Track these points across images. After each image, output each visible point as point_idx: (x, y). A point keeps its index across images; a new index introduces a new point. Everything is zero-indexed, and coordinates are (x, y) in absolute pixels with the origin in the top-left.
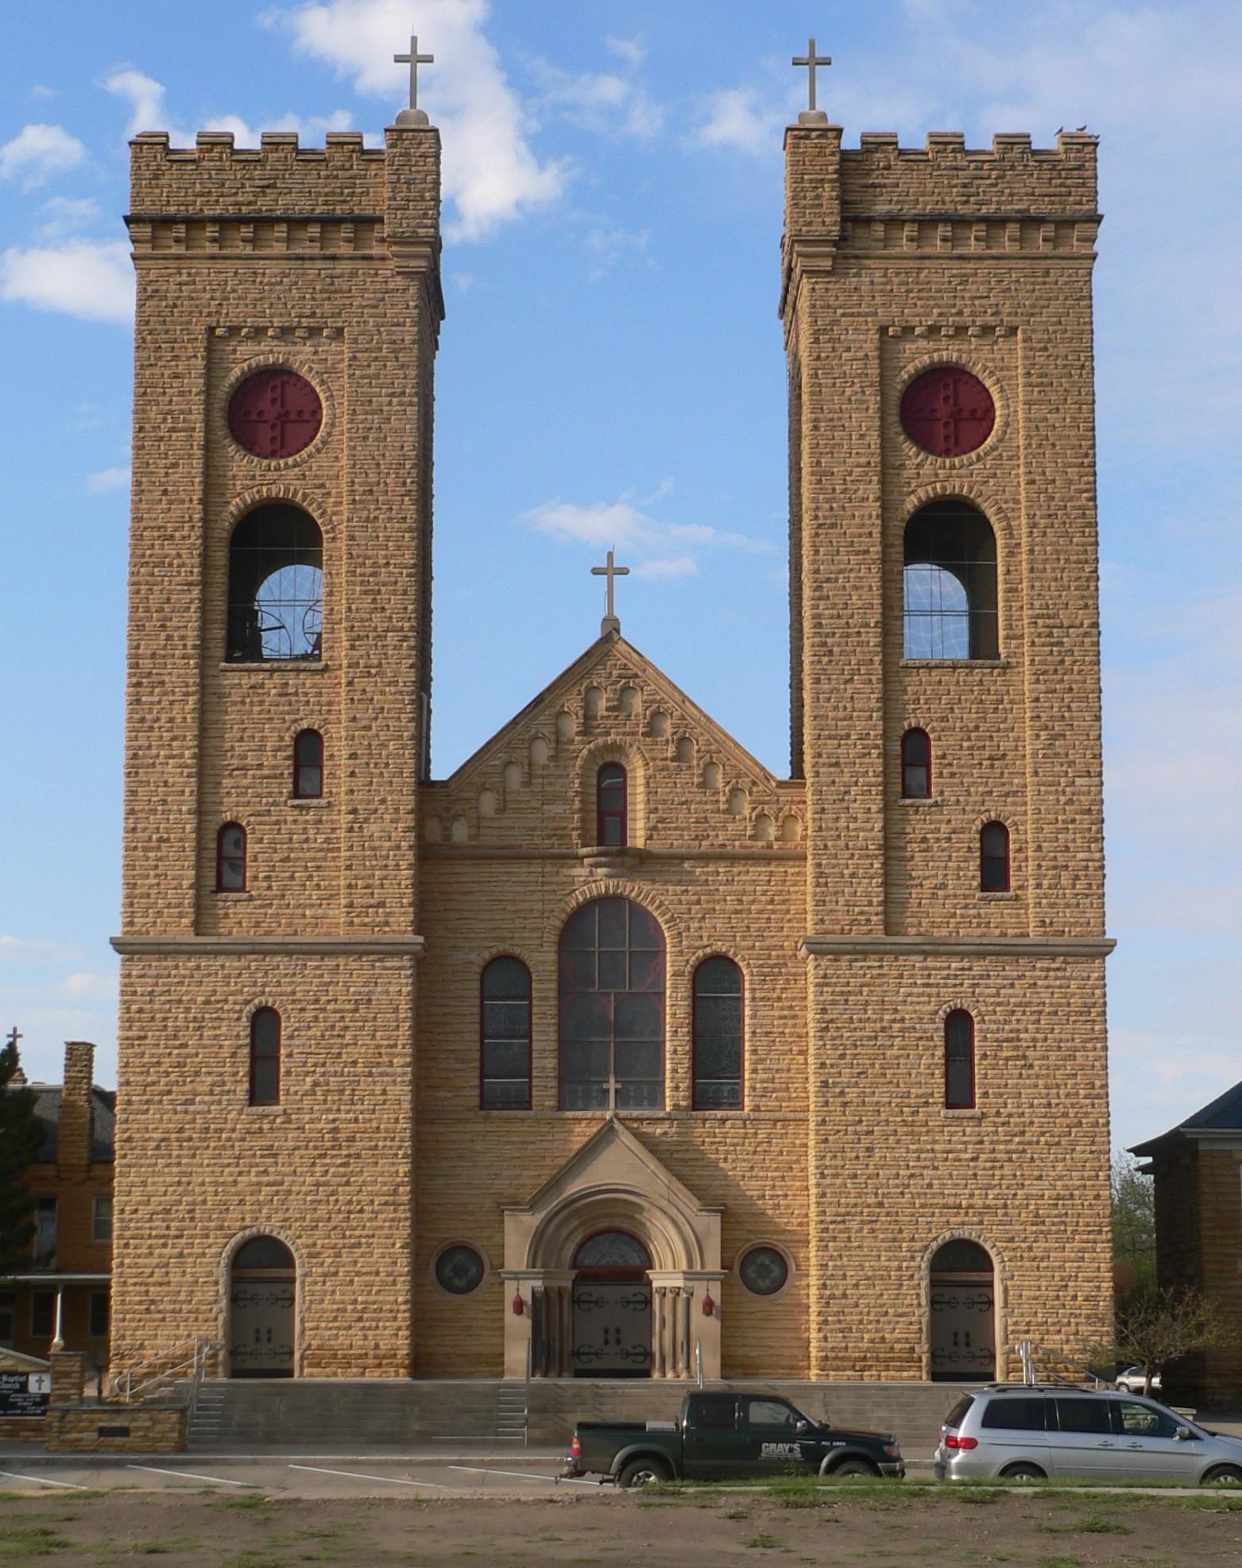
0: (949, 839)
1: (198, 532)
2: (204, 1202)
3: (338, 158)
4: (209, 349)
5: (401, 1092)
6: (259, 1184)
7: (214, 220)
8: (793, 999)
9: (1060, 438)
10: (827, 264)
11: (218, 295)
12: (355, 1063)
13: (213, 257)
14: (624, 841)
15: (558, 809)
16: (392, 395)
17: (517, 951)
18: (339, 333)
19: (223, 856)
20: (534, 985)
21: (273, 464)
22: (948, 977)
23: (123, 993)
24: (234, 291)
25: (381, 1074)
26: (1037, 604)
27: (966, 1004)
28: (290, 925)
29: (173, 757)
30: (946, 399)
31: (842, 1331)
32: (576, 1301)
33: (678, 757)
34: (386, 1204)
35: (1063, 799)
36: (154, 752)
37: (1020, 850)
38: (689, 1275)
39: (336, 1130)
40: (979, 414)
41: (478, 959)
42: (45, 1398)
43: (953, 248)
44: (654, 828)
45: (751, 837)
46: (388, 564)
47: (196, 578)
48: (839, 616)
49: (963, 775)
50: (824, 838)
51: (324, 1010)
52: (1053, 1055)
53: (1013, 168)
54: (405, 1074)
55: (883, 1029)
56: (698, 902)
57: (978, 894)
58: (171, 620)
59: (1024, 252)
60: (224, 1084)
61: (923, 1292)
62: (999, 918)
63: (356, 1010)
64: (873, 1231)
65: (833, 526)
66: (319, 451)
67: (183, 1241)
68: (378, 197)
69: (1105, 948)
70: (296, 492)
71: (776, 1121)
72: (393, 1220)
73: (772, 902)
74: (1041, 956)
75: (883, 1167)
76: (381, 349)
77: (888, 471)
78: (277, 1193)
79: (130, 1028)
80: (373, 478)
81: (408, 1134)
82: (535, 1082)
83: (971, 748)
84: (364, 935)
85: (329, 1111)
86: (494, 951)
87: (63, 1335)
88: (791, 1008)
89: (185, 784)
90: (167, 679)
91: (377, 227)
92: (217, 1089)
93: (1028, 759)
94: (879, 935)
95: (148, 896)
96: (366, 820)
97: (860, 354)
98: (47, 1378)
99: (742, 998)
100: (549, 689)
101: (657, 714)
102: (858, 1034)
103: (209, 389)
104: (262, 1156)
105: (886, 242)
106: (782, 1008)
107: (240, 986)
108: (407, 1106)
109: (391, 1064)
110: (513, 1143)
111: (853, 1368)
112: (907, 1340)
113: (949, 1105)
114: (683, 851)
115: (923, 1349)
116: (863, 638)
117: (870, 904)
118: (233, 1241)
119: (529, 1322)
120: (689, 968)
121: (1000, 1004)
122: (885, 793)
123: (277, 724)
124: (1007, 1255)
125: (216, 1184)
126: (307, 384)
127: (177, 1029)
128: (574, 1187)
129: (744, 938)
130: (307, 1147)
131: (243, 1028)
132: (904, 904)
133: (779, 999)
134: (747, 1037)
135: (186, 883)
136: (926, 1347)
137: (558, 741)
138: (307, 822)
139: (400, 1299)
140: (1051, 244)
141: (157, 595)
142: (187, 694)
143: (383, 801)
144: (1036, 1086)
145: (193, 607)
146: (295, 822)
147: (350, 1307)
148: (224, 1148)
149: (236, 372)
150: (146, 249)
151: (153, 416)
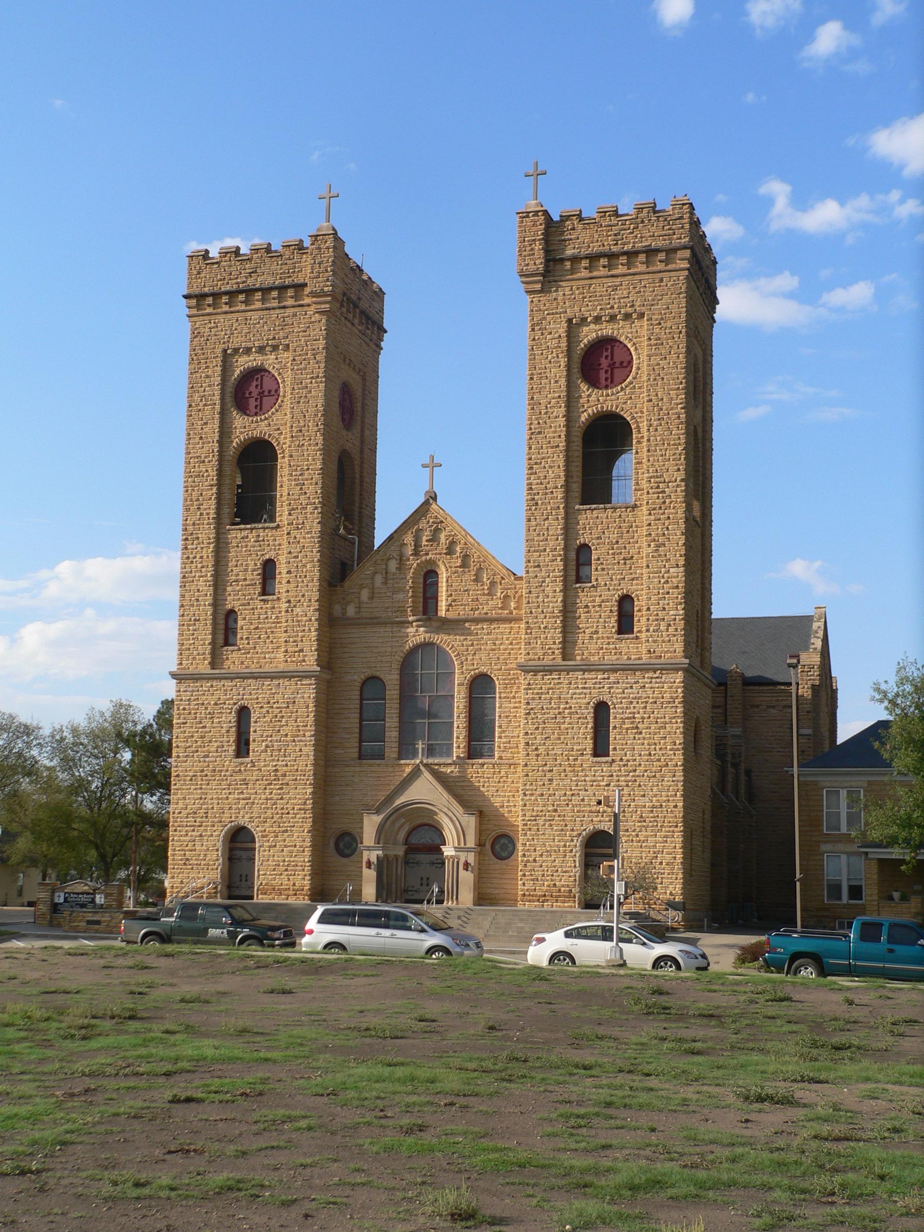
0: (600, 606)
2: (213, 808)
6: (238, 799)
7: (226, 293)
11: (228, 332)
12: (286, 735)
13: (226, 313)
15: (400, 596)
16: (312, 378)
17: (378, 674)
18: (288, 345)
19: (225, 628)
22: (595, 683)
25: (299, 741)
27: (606, 698)
28: (258, 663)
31: (533, 880)
32: (407, 863)
34: (300, 809)
35: (662, 581)
36: (193, 574)
39: (276, 770)
41: (358, 678)
44: (450, 605)
46: (308, 469)
47: (215, 482)
48: (541, 484)
49: (609, 569)
52: (653, 726)
53: (643, 222)
54: (311, 741)
57: (616, 636)
60: (223, 746)
65: (540, 433)
66: (277, 411)
71: (510, 765)
73: (511, 644)
74: (648, 670)
75: (557, 790)
78: (247, 804)
83: (613, 554)
84: (292, 667)
85: (273, 760)
90: (200, 536)
92: (220, 750)
94: (559, 661)
96: (295, 606)
97: (556, 335)
102: (546, 716)
105: (573, 271)
106: (515, 703)
107: (229, 695)
109: (304, 735)
117: (554, 643)
118: (226, 828)
121: (624, 698)
125: (218, 799)
129: (496, 664)
131: (233, 717)
133: (514, 697)
135: (207, 642)
142: (209, 543)
143: (303, 596)
144: (643, 744)
146: (261, 608)
149: (237, 372)
150: (194, 311)
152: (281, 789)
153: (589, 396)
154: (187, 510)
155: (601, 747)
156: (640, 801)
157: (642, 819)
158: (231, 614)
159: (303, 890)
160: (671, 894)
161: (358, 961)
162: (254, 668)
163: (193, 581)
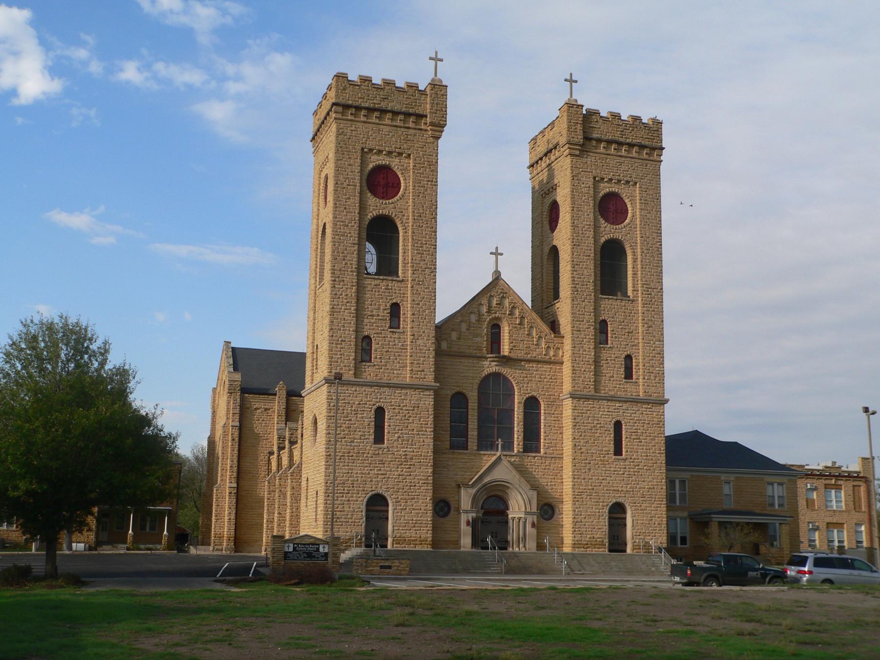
1: (357, 225)
3: (411, 91)
5: (430, 441)
7: (366, 108)
10: (577, 152)
13: (365, 122)
14: (499, 353)
15: (479, 339)
18: (409, 155)
19: (364, 348)
27: (620, 418)
32: (482, 522)
38: (526, 513)
39: (406, 455)
41: (450, 393)
42: (326, 554)
47: (356, 242)
61: (607, 520)
62: (630, 390)
68: (427, 108)
74: (645, 403)
77: (596, 227)
80: (421, 211)
84: (416, 382)
94: (593, 393)
98: (327, 546)
100: (477, 295)
101: (513, 307)
103: (362, 171)
105: (596, 147)
107: (371, 398)
108: (432, 447)
115: (606, 541)
118: (368, 496)
123: (384, 300)
124: (633, 508)
125: (362, 474)
127: (348, 414)
128: (487, 479)
131: (372, 415)
135: (351, 358)
137: (480, 315)
149: (371, 166)
150: (340, 116)
155: (618, 451)
156: (642, 485)
157: (643, 496)
158: (367, 339)
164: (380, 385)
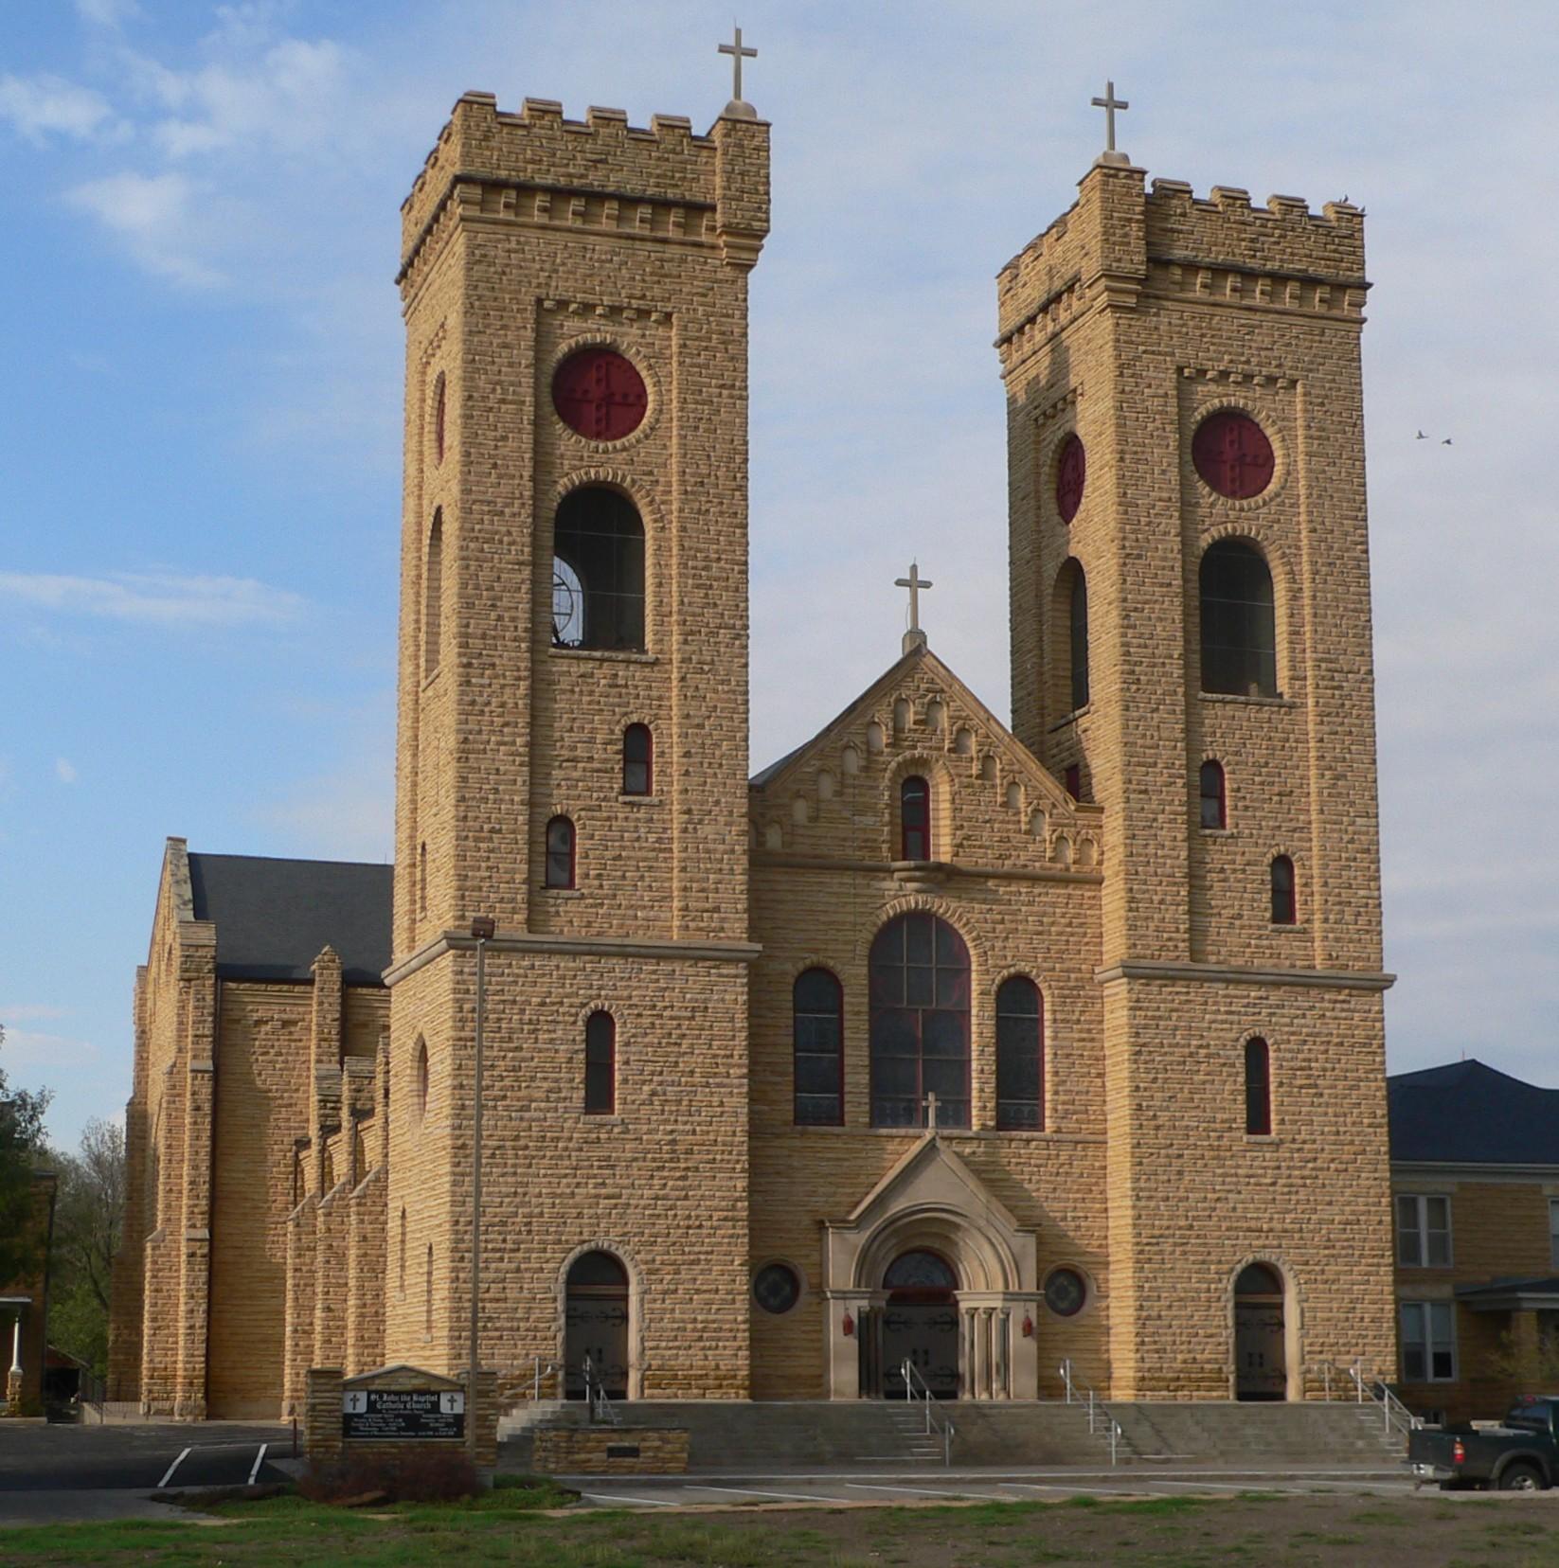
0: (1244, 871)
2: (541, 1214)
3: (670, 140)
4: (537, 322)
6: (597, 1196)
8: (1091, 1022)
9: (1338, 490)
10: (1132, 301)
11: (547, 266)
12: (692, 1072)
13: (543, 227)
15: (869, 820)
16: (722, 386)
17: (831, 963)
18: (668, 316)
19: (554, 847)
20: (846, 999)
21: (601, 446)
22: (1247, 1005)
23: (455, 991)
24: (564, 264)
25: (718, 1085)
26: (1320, 647)
28: (621, 926)
29: (504, 744)
30: (1232, 442)
31: (1157, 1351)
32: (887, 1323)
33: (983, 775)
34: (725, 1219)
35: (1346, 838)
36: (485, 737)
37: (1306, 885)
38: (1009, 1296)
39: (674, 1142)
40: (1260, 461)
41: (792, 969)
43: (1242, 298)
44: (961, 845)
45: (1051, 859)
46: (719, 559)
47: (526, 557)
48: (1146, 646)
49: (1255, 809)
50: (1135, 864)
51: (661, 1016)
52: (1341, 1084)
53: (1293, 230)
54: (741, 1086)
55: (1191, 1055)
56: (1002, 922)
57: (1271, 926)
58: (501, 599)
59: (1212, 299)
60: (560, 1090)
62: (1286, 951)
63: (693, 1018)
64: (1184, 1253)
65: (1139, 557)
66: (647, 437)
67: (520, 1255)
69: (1381, 984)
70: (624, 477)
71: (1077, 1143)
72: (731, 1236)
73: (1070, 925)
74: (1328, 987)
75: (1192, 1190)
76: (710, 339)
77: (1187, 506)
78: (615, 1206)
79: (463, 1029)
81: (745, 1148)
82: (847, 1098)
83: (1262, 783)
84: (699, 940)
85: (666, 1122)
86: (808, 962)
87: (20, 1363)
88: (1089, 1031)
89: (517, 773)
90: (497, 661)
91: (708, 215)
92: (553, 1096)
93: (1313, 797)
94: (1185, 962)
95: (480, 889)
96: (700, 822)
97: (1161, 392)
99: (1042, 1019)
100: (862, 698)
101: (962, 730)
102: (1168, 1058)
103: (538, 362)
104: (600, 1167)
105: (1183, 286)
106: (1081, 1031)
108: (744, 1119)
109: (728, 1076)
110: (829, 1159)
111: (1168, 1389)
112: (1216, 1361)
113: (1250, 1131)
114: (989, 869)
115: (1230, 1368)
116: (1168, 668)
117: (1177, 930)
118: (572, 1256)
119: (856, 1342)
120: (994, 988)
121: (1293, 1034)
122: (1189, 822)
124: (1303, 1278)
125: (554, 1195)
126: (632, 368)
127: (511, 1031)
128: (898, 1206)
129: (1045, 959)
130: (644, 1159)
131: (579, 1032)
132: (1205, 932)
133: (1078, 1021)
134: (1047, 1058)
135: (519, 878)
136: (1233, 1368)
137: (870, 752)
138: (638, 820)
139: (740, 1318)
140: (546, 215)
141: (486, 572)
142: (519, 679)
143: (717, 803)
144: (1326, 1114)
145: (525, 588)
146: (626, 819)
147: (690, 1326)
148: (561, 1158)
149: (563, 348)
151: (481, 384)
152: (684, 1178)
153: (1212, 505)
154: (470, 606)
155: (1258, 1121)
158: (562, 823)
159: (734, 1377)
160: (1380, 1372)
161: (552, 1519)
162: (612, 938)
163: (484, 751)
164: (598, 952)
